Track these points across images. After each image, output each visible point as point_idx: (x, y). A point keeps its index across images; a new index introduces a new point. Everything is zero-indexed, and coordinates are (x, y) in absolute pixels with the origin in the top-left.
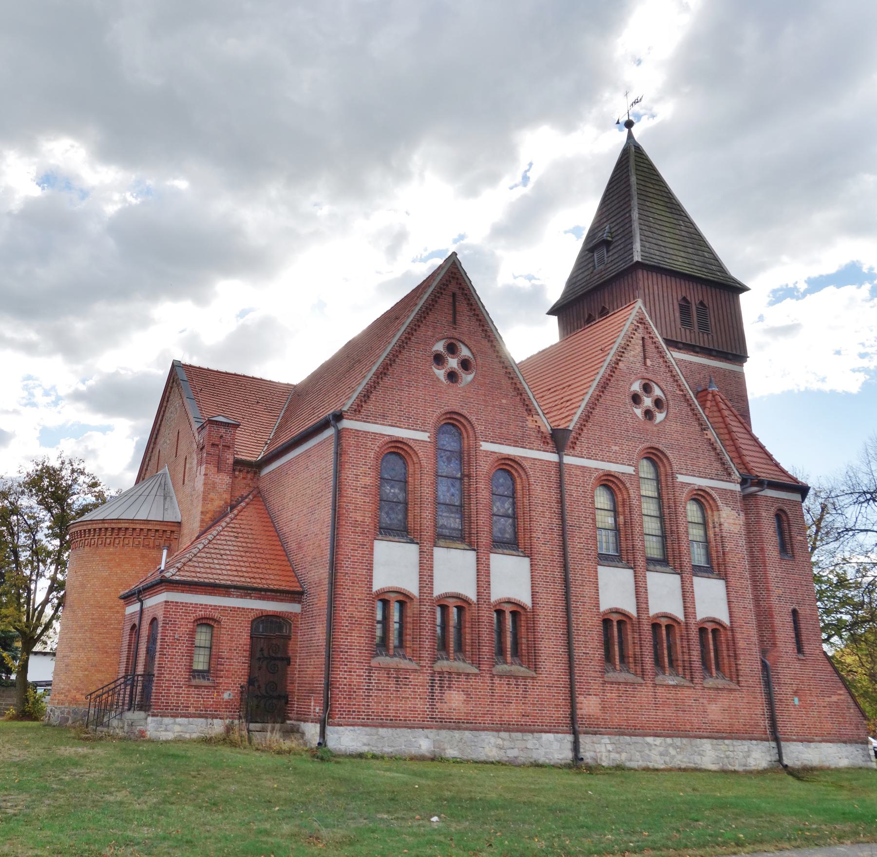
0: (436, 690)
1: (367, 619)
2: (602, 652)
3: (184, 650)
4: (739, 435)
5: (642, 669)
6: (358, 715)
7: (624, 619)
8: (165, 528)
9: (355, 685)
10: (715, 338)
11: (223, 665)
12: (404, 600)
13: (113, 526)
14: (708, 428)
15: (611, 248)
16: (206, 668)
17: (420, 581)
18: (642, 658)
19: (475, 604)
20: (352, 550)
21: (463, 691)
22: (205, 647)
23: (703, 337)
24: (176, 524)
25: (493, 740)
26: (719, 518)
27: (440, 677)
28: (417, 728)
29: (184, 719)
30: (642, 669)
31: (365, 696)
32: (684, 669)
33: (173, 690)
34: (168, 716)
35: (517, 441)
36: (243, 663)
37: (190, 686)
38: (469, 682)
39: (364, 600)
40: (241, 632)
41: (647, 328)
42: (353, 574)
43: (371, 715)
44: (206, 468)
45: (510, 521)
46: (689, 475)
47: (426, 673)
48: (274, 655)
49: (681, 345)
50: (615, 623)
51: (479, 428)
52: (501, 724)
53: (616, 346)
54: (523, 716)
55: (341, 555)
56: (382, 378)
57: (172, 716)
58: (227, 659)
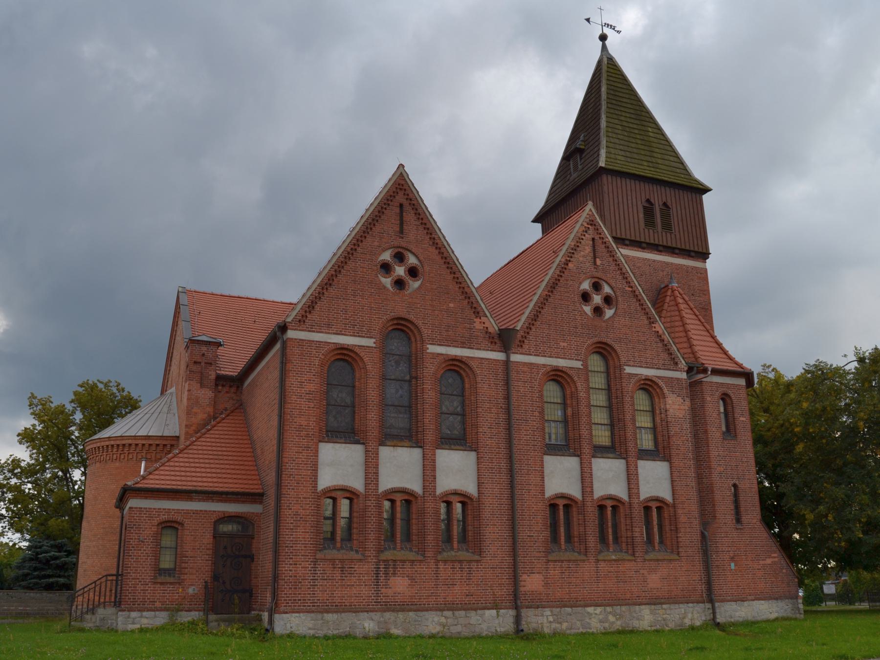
0: (381, 577)
1: (312, 516)
2: (547, 533)
3: (149, 551)
4: (692, 327)
5: (586, 547)
6: (304, 603)
7: (569, 503)
8: (165, 442)
9: (300, 576)
10: (678, 237)
11: (187, 563)
12: (351, 495)
13: (118, 442)
14: (657, 321)
15: (584, 155)
16: (172, 566)
17: (366, 478)
18: (585, 537)
19: (421, 497)
20: (296, 452)
21: (408, 577)
22: (171, 548)
23: (649, 232)
24: (175, 438)
25: (436, 619)
26: (665, 404)
27: (385, 565)
28: (362, 612)
29: (150, 612)
30: (586, 547)
31: (311, 585)
32: (627, 545)
33: (140, 587)
34: (135, 611)
35: (465, 343)
36: (207, 560)
37: (155, 583)
38: (414, 568)
39: (309, 498)
40: (203, 533)
41: (597, 229)
42: (297, 475)
43: (316, 603)
44: (189, 384)
45: (459, 418)
46: (636, 366)
47: (371, 562)
48: (237, 553)
49: (644, 245)
50: (561, 507)
51: (426, 332)
52: (445, 604)
53: (565, 248)
54: (467, 595)
55: (285, 457)
56: (327, 289)
57: (139, 611)
58: (190, 557)
